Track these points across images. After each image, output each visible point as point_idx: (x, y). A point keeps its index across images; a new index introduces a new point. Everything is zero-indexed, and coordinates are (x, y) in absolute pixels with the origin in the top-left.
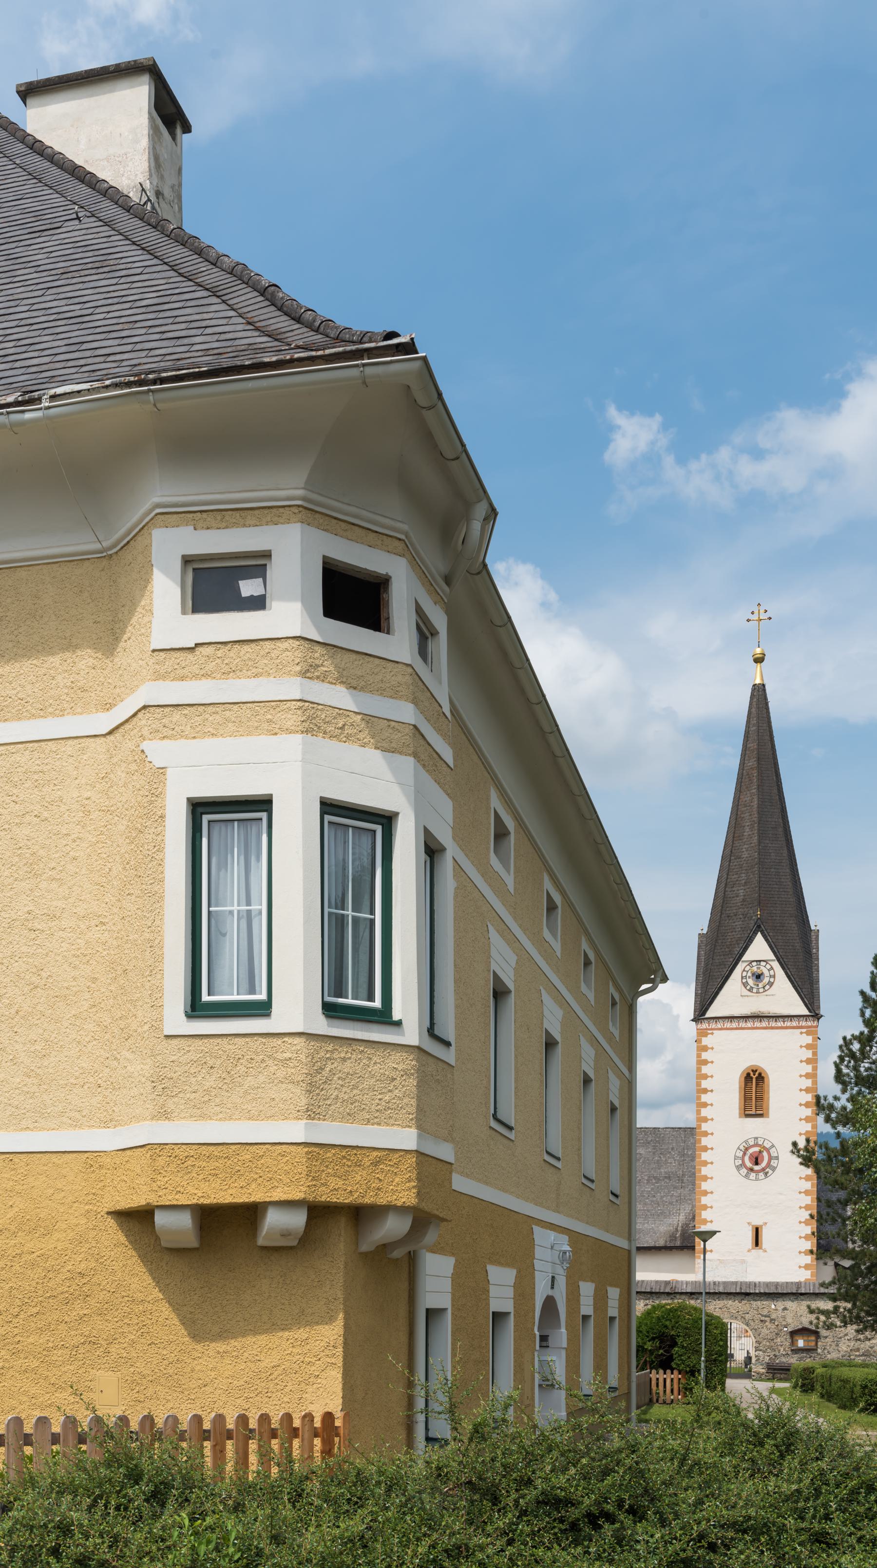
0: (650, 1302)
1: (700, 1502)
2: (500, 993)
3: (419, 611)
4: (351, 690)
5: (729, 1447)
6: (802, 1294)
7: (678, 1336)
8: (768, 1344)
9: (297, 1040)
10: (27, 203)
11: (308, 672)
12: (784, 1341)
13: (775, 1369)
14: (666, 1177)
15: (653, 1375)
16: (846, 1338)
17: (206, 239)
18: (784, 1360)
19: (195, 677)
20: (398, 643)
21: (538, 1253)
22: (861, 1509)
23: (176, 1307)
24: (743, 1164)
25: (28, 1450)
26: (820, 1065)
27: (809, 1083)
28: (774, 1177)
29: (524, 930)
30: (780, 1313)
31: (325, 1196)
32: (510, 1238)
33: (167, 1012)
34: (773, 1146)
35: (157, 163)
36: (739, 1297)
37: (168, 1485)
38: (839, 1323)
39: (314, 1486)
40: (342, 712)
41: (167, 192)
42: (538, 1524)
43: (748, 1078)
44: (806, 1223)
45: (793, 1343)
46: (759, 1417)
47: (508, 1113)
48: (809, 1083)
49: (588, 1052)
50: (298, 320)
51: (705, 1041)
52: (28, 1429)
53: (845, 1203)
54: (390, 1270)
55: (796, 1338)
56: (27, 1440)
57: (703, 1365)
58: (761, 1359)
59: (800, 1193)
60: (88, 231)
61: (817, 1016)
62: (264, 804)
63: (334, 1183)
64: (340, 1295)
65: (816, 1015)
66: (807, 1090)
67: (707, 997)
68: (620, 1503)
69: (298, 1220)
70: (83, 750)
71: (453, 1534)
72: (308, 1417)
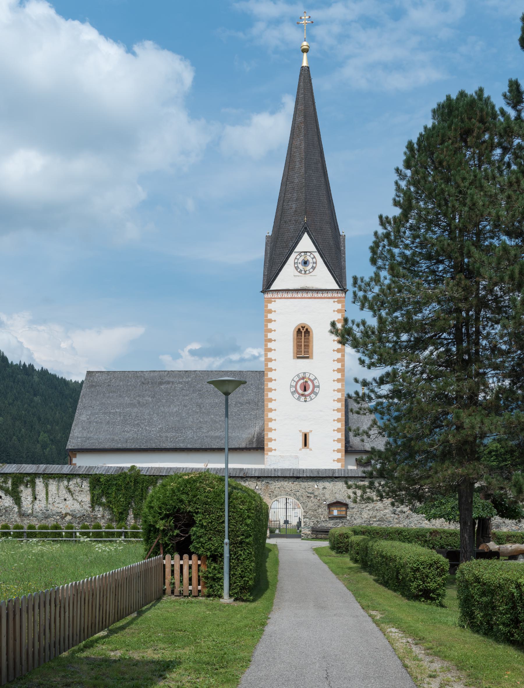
4: (392, 601)
6: (336, 477)
7: (197, 513)
8: (312, 513)
12: (323, 512)
13: (317, 531)
14: (247, 403)
15: (167, 561)
16: (367, 508)
18: (323, 524)
24: (296, 391)
30: (321, 491)
34: (316, 378)
36: (292, 479)
38: (375, 498)
43: (299, 332)
45: (330, 512)
55: (332, 509)
57: (226, 549)
58: (308, 524)
59: (334, 410)
67: (272, 276)
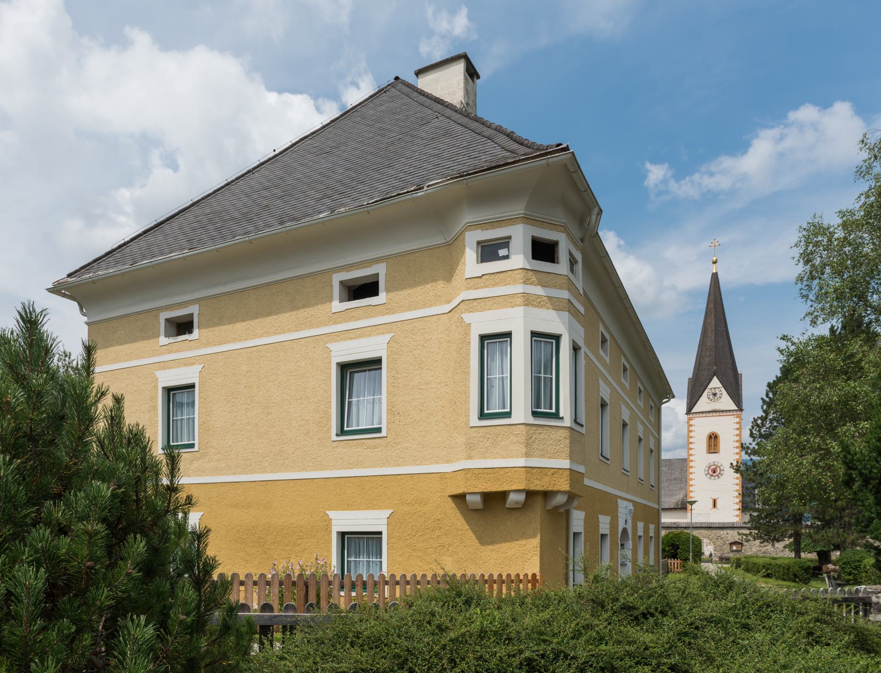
0: (667, 531)
1: (691, 609)
2: (603, 405)
3: (570, 254)
5: (704, 587)
9: (521, 426)
10: (418, 115)
11: (526, 282)
12: (727, 548)
15: (669, 561)
17: (486, 118)
19: (482, 287)
20: (562, 268)
21: (620, 510)
22: (764, 615)
23: (474, 532)
25: (419, 587)
26: (743, 431)
27: (738, 438)
28: (722, 478)
29: (614, 379)
31: (533, 487)
32: (608, 504)
33: (471, 417)
35: (467, 92)
37: (472, 599)
39: (529, 600)
40: (539, 296)
41: (471, 103)
42: (621, 617)
43: (710, 437)
44: (737, 497)
45: (731, 548)
46: (717, 575)
47: (607, 453)
48: (738, 438)
49: (640, 428)
50: (522, 144)
51: (691, 422)
52: (419, 578)
53: (754, 488)
54: (559, 517)
56: (418, 583)
60: (442, 122)
61: (741, 410)
62: (508, 335)
63: (536, 482)
64: (539, 526)
65: (741, 409)
66: (737, 441)
68: (656, 609)
69: (522, 497)
70: (439, 319)
71: (585, 620)
72: (526, 575)
